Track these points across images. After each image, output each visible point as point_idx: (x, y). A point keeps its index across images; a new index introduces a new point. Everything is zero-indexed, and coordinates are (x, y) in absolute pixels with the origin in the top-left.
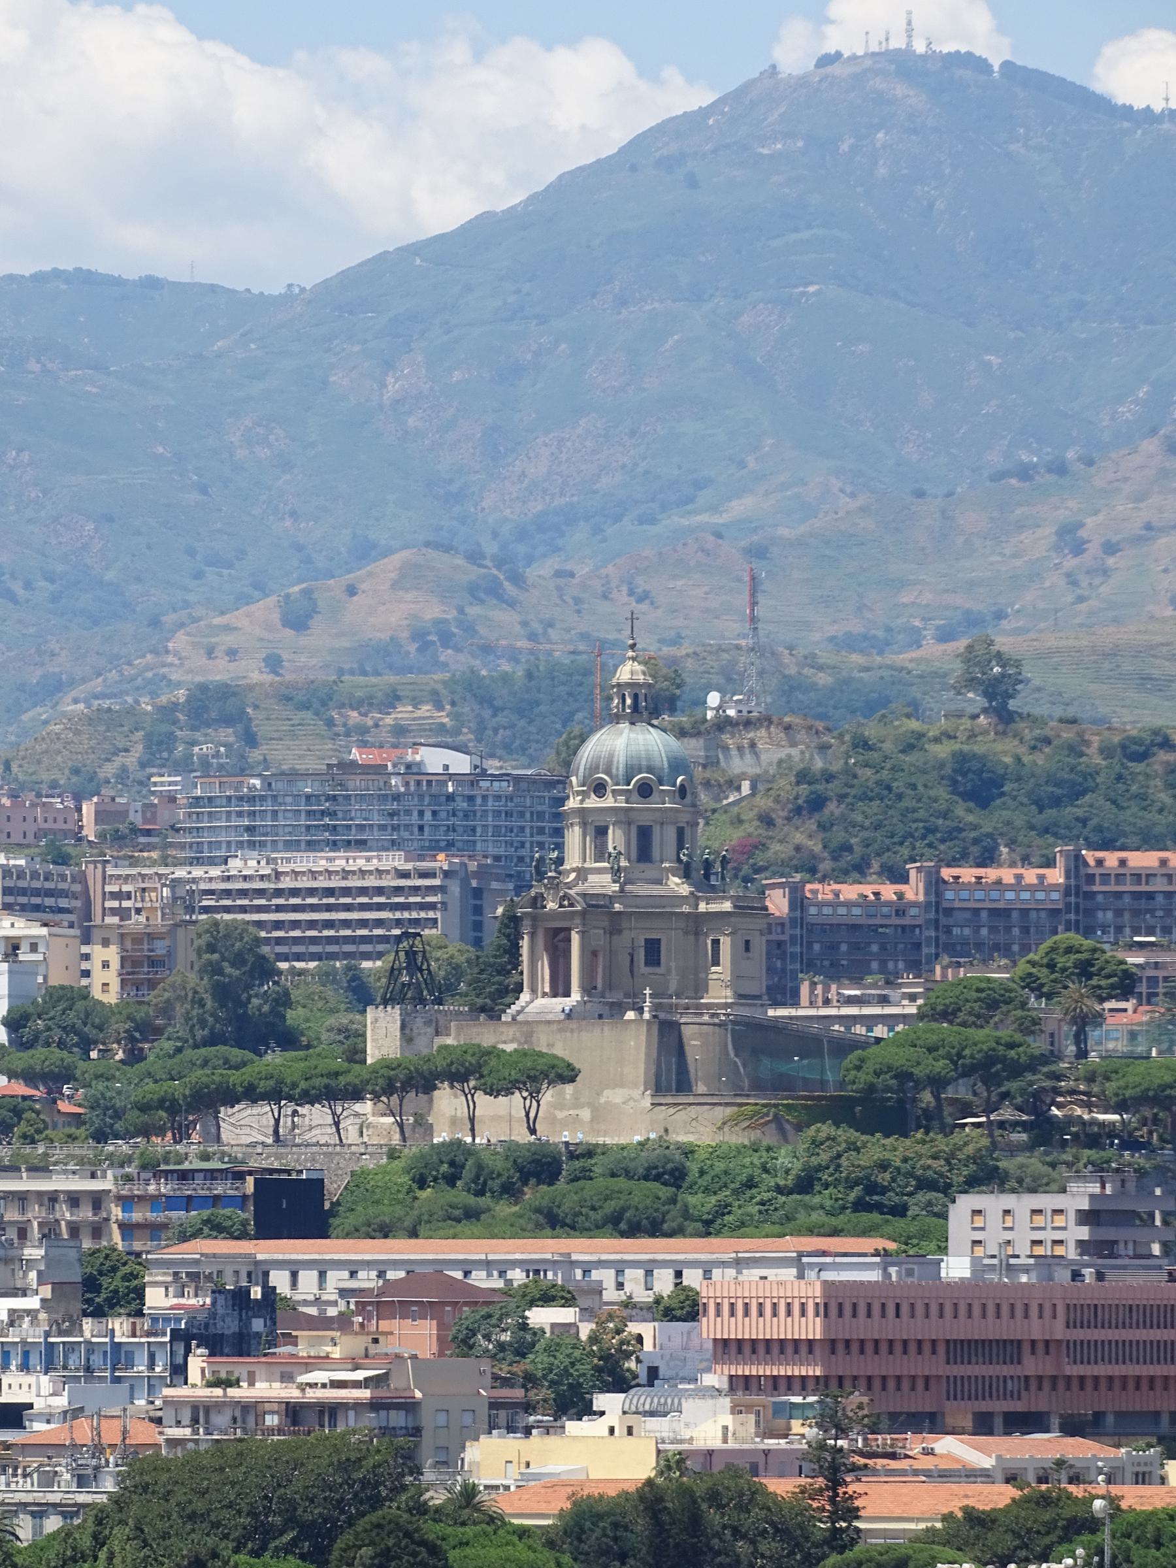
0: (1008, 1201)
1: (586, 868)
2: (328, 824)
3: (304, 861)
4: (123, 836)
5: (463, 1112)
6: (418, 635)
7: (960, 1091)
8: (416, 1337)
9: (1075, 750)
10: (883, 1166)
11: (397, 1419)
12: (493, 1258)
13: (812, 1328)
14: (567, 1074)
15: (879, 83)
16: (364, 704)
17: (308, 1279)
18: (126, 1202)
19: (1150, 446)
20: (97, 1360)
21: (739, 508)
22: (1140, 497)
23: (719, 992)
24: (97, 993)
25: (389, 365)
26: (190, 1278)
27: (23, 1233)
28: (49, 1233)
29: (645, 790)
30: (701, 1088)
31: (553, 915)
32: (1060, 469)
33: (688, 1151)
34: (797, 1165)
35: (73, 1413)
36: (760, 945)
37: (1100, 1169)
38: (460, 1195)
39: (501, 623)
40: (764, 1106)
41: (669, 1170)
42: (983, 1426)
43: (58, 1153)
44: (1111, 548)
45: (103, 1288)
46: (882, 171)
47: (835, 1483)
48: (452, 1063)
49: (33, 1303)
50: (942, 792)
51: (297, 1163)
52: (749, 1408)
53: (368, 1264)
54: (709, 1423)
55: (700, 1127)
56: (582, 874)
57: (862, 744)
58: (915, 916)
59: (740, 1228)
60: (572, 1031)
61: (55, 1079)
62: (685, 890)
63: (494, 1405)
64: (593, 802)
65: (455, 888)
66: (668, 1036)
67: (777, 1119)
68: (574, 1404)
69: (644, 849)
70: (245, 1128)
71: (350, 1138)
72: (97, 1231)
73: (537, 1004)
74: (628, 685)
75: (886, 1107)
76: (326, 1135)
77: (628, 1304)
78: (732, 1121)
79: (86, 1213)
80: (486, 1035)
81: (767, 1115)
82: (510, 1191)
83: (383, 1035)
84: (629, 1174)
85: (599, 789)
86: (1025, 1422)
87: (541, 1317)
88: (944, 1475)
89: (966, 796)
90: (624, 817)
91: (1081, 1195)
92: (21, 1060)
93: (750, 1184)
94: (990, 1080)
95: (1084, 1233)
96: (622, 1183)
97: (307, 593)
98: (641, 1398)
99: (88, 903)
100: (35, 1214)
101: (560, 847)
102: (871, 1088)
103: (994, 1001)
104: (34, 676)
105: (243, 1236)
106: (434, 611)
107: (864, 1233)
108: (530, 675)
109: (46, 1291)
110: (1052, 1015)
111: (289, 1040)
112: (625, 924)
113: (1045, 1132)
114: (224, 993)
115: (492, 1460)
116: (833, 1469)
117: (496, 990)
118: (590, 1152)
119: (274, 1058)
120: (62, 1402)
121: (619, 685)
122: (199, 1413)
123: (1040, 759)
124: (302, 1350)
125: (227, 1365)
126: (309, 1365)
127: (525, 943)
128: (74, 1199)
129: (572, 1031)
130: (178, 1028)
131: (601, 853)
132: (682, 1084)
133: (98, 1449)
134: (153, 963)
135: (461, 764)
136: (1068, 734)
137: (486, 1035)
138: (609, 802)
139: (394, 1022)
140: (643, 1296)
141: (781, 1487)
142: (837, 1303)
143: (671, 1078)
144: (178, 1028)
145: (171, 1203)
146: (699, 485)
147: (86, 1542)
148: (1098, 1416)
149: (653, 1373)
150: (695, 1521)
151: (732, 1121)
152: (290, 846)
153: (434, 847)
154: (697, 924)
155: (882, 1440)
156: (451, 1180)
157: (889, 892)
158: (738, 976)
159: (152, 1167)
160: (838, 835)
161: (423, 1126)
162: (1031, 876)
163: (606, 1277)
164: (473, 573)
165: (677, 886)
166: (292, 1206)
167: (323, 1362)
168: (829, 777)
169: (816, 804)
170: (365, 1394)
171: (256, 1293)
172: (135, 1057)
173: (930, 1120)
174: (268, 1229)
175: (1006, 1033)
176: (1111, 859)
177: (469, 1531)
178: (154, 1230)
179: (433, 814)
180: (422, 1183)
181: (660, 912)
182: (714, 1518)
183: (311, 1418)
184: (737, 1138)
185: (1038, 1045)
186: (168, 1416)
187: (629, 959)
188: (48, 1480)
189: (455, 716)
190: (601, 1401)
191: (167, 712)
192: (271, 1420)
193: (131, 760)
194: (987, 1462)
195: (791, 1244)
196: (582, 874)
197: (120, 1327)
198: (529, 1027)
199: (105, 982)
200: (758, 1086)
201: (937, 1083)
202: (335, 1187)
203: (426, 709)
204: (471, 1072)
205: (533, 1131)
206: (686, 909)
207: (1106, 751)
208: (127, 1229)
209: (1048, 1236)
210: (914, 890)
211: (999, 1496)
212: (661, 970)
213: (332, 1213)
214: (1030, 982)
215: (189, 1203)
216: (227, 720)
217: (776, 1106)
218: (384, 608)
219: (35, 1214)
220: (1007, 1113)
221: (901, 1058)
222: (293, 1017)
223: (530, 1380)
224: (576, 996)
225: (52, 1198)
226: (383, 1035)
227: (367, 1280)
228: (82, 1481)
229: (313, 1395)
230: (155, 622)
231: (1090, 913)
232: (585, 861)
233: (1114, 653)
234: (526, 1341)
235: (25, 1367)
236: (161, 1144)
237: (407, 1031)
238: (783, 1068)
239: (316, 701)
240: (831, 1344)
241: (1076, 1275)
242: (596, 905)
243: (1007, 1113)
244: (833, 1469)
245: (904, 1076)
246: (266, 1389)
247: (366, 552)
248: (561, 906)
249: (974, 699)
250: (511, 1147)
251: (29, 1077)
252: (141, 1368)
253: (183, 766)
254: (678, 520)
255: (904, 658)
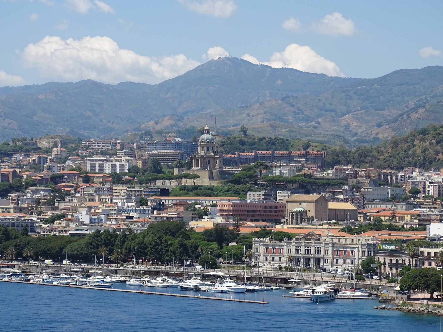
0: (254, 193)
1: (201, 152)
2: (165, 147)
3: (162, 151)
4: (139, 148)
5: (186, 181)
6: (171, 125)
7: (246, 180)
8: (182, 209)
9: (254, 139)
10: (238, 189)
11: (180, 219)
12: (190, 199)
13: (231, 208)
14: (198, 177)
15: (225, 61)
16: (166, 133)
17: (167, 201)
18: (145, 192)
19: (258, 104)
20: (142, 211)
21: (208, 111)
22: (257, 110)
23: (217, 167)
24: (139, 166)
25: (167, 93)
26: (153, 201)
27: (132, 195)
28: (135, 195)
29: (208, 142)
30: (215, 179)
32: (247, 107)
33: (213, 186)
34: (227, 189)
35: (139, 218)
36: (222, 161)
37: (266, 189)
38: (185, 191)
39: (181, 124)
41: (211, 188)
42: (251, 220)
43: (136, 186)
44: (253, 116)
45: (142, 202)
46: (226, 71)
47: (237, 227)
49: (134, 204)
50: (238, 144)
51: (165, 187)
52: (224, 218)
53: (174, 200)
54: (220, 220)
55: (215, 184)
56: (200, 152)
57: (229, 138)
58: (236, 159)
59: (220, 196)
61: (134, 177)
62: (213, 154)
63: (192, 217)
65: (180, 155)
66: (211, 172)
68: (201, 217)
69: (208, 150)
70: (159, 183)
71: (172, 184)
72: (141, 195)
73: (194, 168)
75: (238, 181)
76: (169, 184)
77: (207, 205)
78: (219, 183)
79: (139, 193)
80: (188, 172)
82: (192, 191)
83: (176, 172)
84: (206, 189)
85: (203, 142)
86: (257, 220)
87: (197, 206)
88: (248, 227)
89: (241, 144)
90: (206, 145)
91: (263, 192)
92: (130, 174)
93: (221, 190)
94: (250, 178)
95: (263, 197)
96: (205, 190)
97: (158, 120)
98: (209, 216)
99: (135, 155)
100: (133, 193)
101: (198, 149)
102: (236, 179)
103: (251, 169)
104: (125, 130)
105: (159, 196)
106: (173, 122)
107: (235, 197)
108: (185, 130)
109: (135, 202)
110: (257, 170)
111: (163, 172)
113: (257, 184)
114: (155, 167)
115: (193, 224)
116: (237, 226)
117: (190, 166)
118: (201, 186)
119: (161, 174)
120: (138, 216)
122: (156, 218)
123: (250, 140)
124: (169, 210)
125: (159, 212)
126: (169, 212)
127: (193, 161)
128: (138, 191)
130: (149, 171)
131: (203, 150)
132: (213, 178)
133: (144, 222)
134: (146, 163)
135: (180, 140)
136: (253, 137)
137: (188, 172)
138: (204, 144)
140: (208, 204)
141: (231, 228)
142: (234, 205)
143: (211, 177)
144: (149, 171)
145: (150, 192)
146: (204, 108)
147: (146, 234)
148: (265, 219)
149: (210, 213)
150: (222, 232)
151: (219, 183)
152: (160, 149)
153: (177, 150)
154: (214, 159)
155: (241, 222)
156: (184, 190)
157: (233, 156)
158: (219, 165)
159: (147, 187)
160: (226, 149)
161: (181, 183)
162: (250, 154)
163: (204, 202)
164: (177, 118)
165: (212, 154)
166: (165, 192)
167: (171, 212)
168: (225, 142)
169: (223, 145)
170: (177, 216)
171: (161, 203)
172: (143, 174)
173: (243, 183)
174: (162, 195)
175: (252, 172)
176: (260, 152)
177: (192, 233)
178: (148, 195)
179: (177, 146)
180: (181, 190)
181: (210, 157)
182: (224, 232)
183: (170, 219)
184: (220, 185)
185: (256, 174)
186: (152, 218)
187: (206, 163)
188: (138, 226)
189: (176, 135)
190: (204, 217)
191: (142, 134)
192: (165, 219)
193: (138, 139)
194: (254, 225)
195: (227, 198)
196: (200, 152)
197: (145, 207)
198: (194, 171)
199: (140, 165)
200: (222, 179)
201: (244, 178)
202: (170, 190)
203: (173, 134)
204: (187, 176)
207: (258, 139)
208: (144, 195)
209: (259, 197)
210: (236, 156)
211: (258, 229)
213: (170, 193)
214: (255, 166)
215: (152, 192)
216: (149, 135)
218: (167, 122)
219: (133, 193)
220: (252, 182)
221: (240, 175)
222: (163, 170)
223: (196, 214)
224: (200, 167)
225: (135, 191)
226: (176, 172)
227: (174, 202)
228: (142, 226)
229: (170, 216)
230: (139, 123)
231: (257, 159)
233: (255, 128)
234: (195, 209)
235: (133, 212)
236: (148, 185)
238: (225, 176)
239: (160, 133)
240: (233, 210)
241: (263, 202)
242: (202, 156)
243: (252, 182)
244: (237, 226)
245: (240, 178)
246: (164, 215)
247: (164, 116)
249: (242, 133)
250: (192, 185)
251: (131, 177)
252: (147, 212)
253: (144, 140)
254: (201, 112)
255: (229, 129)
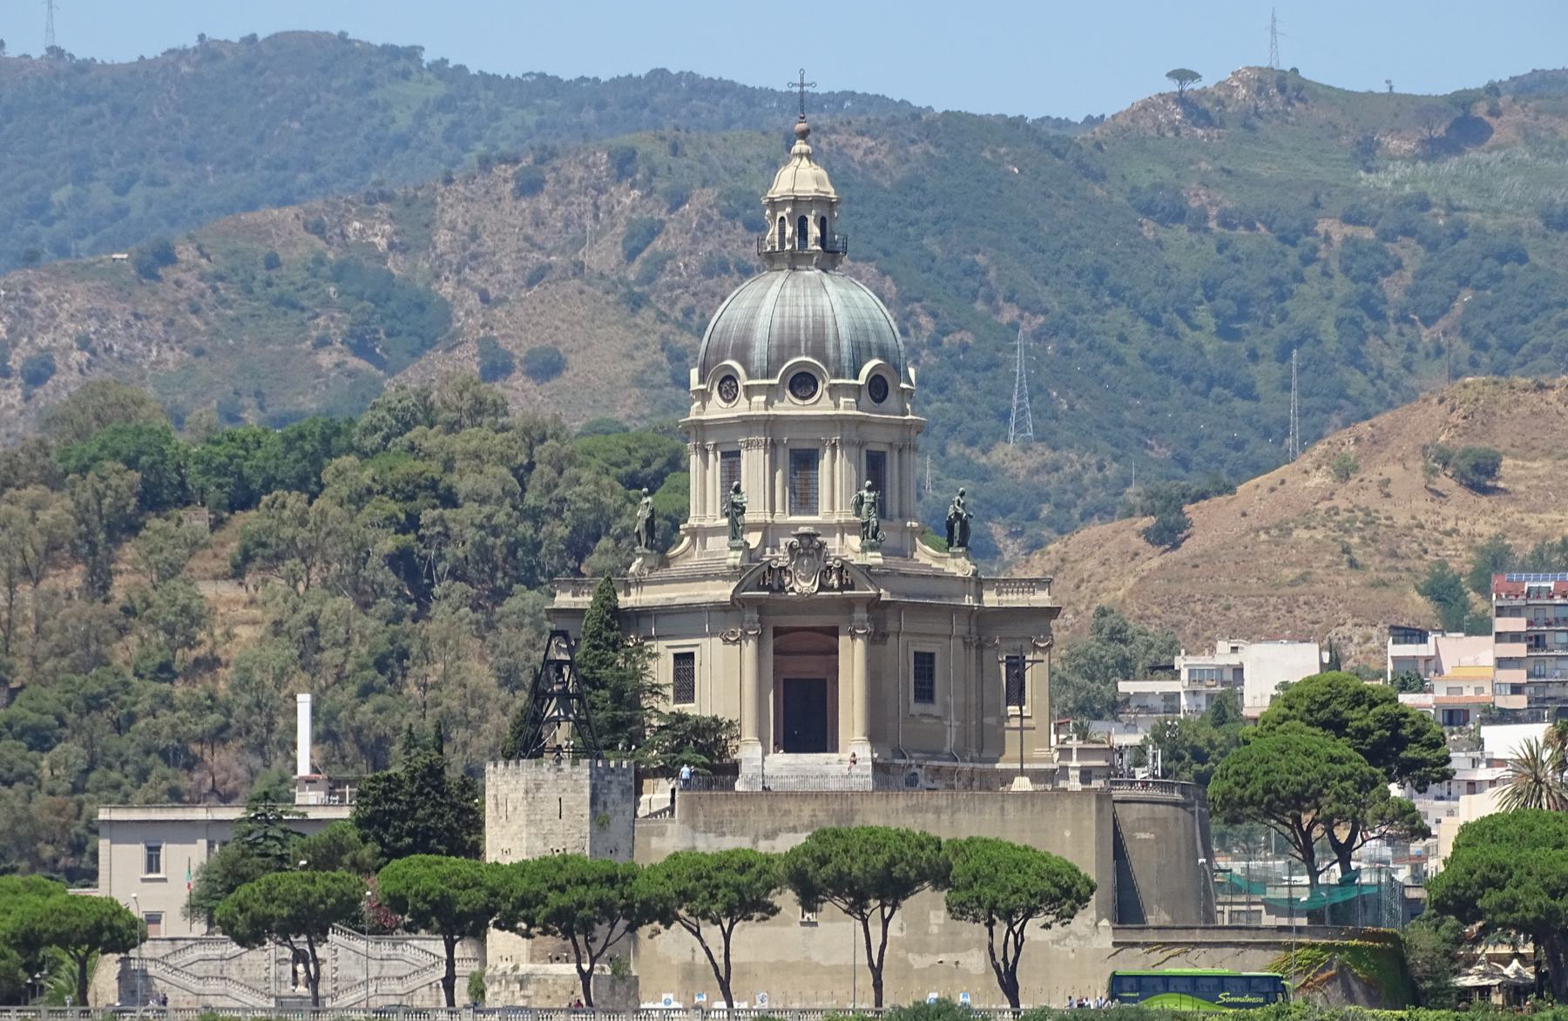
29: (878, 388)
31: (807, 604)
40: (1325, 948)
48: (892, 863)
60: (938, 811)
64: (790, 406)
67: (1343, 975)
74: (818, 201)
81: (1329, 965)
85: (803, 383)
90: (846, 431)
112: (891, 626)
121: (795, 201)
129: (938, 811)
138: (821, 406)
139: (577, 789)
181: (933, 603)
205: (1010, 987)
206: (969, 601)
212: (935, 709)
217: (1340, 949)
232: (773, 512)
237: (600, 808)
248: (822, 587)
